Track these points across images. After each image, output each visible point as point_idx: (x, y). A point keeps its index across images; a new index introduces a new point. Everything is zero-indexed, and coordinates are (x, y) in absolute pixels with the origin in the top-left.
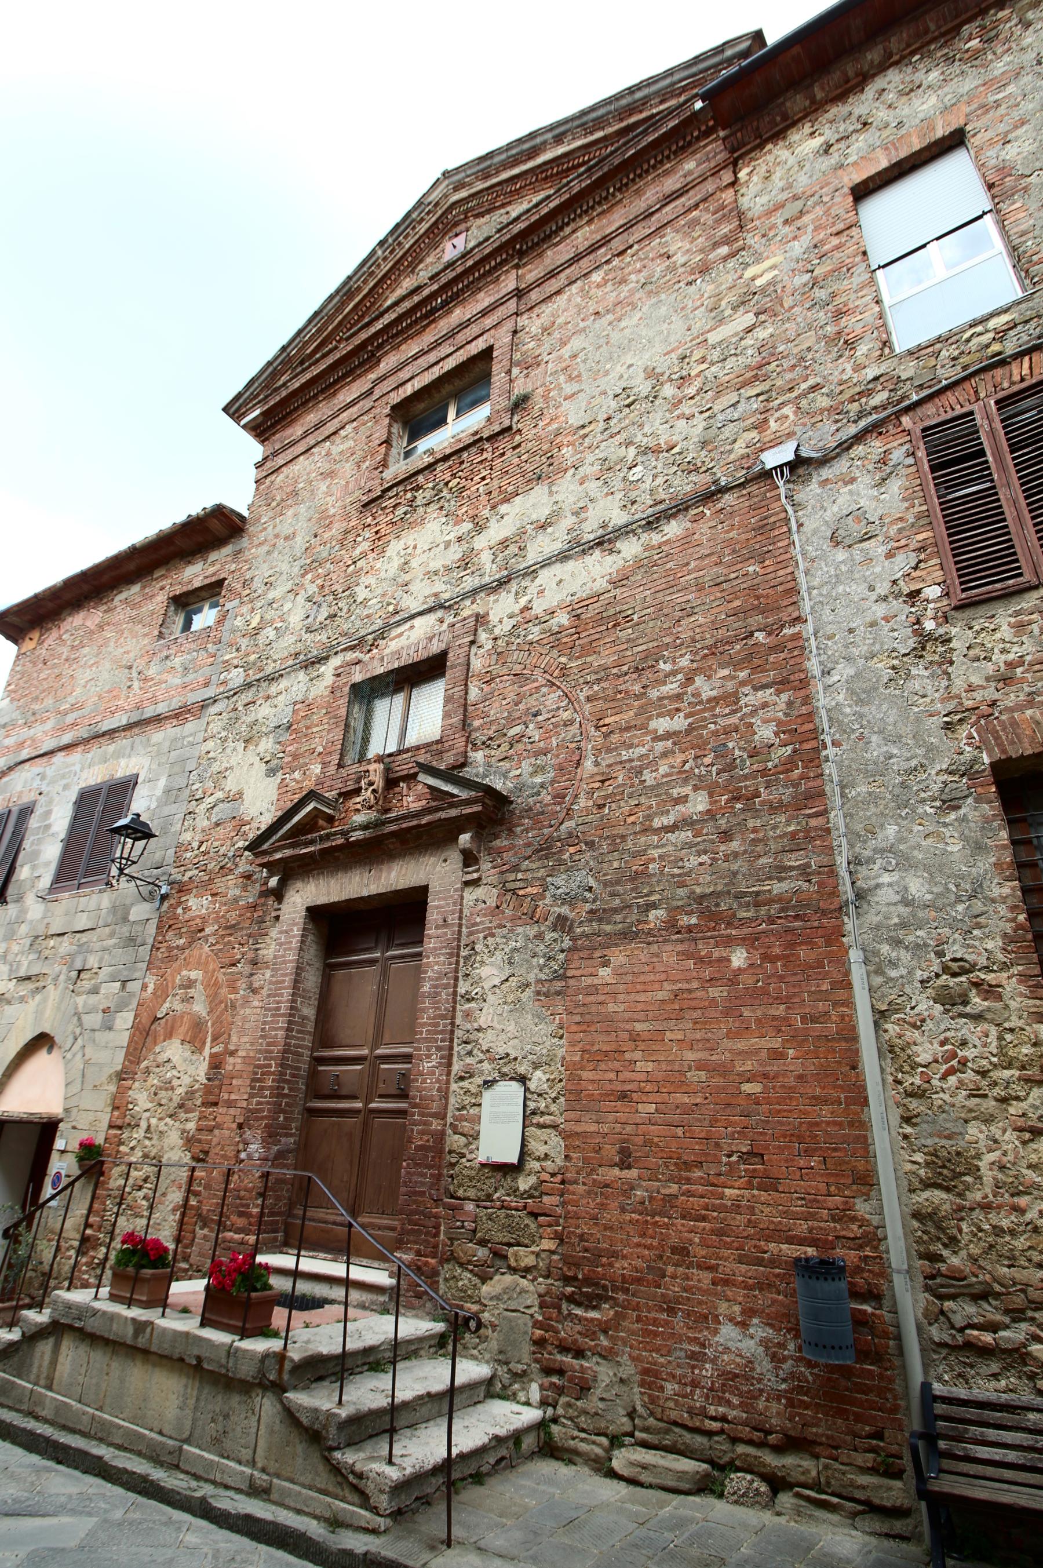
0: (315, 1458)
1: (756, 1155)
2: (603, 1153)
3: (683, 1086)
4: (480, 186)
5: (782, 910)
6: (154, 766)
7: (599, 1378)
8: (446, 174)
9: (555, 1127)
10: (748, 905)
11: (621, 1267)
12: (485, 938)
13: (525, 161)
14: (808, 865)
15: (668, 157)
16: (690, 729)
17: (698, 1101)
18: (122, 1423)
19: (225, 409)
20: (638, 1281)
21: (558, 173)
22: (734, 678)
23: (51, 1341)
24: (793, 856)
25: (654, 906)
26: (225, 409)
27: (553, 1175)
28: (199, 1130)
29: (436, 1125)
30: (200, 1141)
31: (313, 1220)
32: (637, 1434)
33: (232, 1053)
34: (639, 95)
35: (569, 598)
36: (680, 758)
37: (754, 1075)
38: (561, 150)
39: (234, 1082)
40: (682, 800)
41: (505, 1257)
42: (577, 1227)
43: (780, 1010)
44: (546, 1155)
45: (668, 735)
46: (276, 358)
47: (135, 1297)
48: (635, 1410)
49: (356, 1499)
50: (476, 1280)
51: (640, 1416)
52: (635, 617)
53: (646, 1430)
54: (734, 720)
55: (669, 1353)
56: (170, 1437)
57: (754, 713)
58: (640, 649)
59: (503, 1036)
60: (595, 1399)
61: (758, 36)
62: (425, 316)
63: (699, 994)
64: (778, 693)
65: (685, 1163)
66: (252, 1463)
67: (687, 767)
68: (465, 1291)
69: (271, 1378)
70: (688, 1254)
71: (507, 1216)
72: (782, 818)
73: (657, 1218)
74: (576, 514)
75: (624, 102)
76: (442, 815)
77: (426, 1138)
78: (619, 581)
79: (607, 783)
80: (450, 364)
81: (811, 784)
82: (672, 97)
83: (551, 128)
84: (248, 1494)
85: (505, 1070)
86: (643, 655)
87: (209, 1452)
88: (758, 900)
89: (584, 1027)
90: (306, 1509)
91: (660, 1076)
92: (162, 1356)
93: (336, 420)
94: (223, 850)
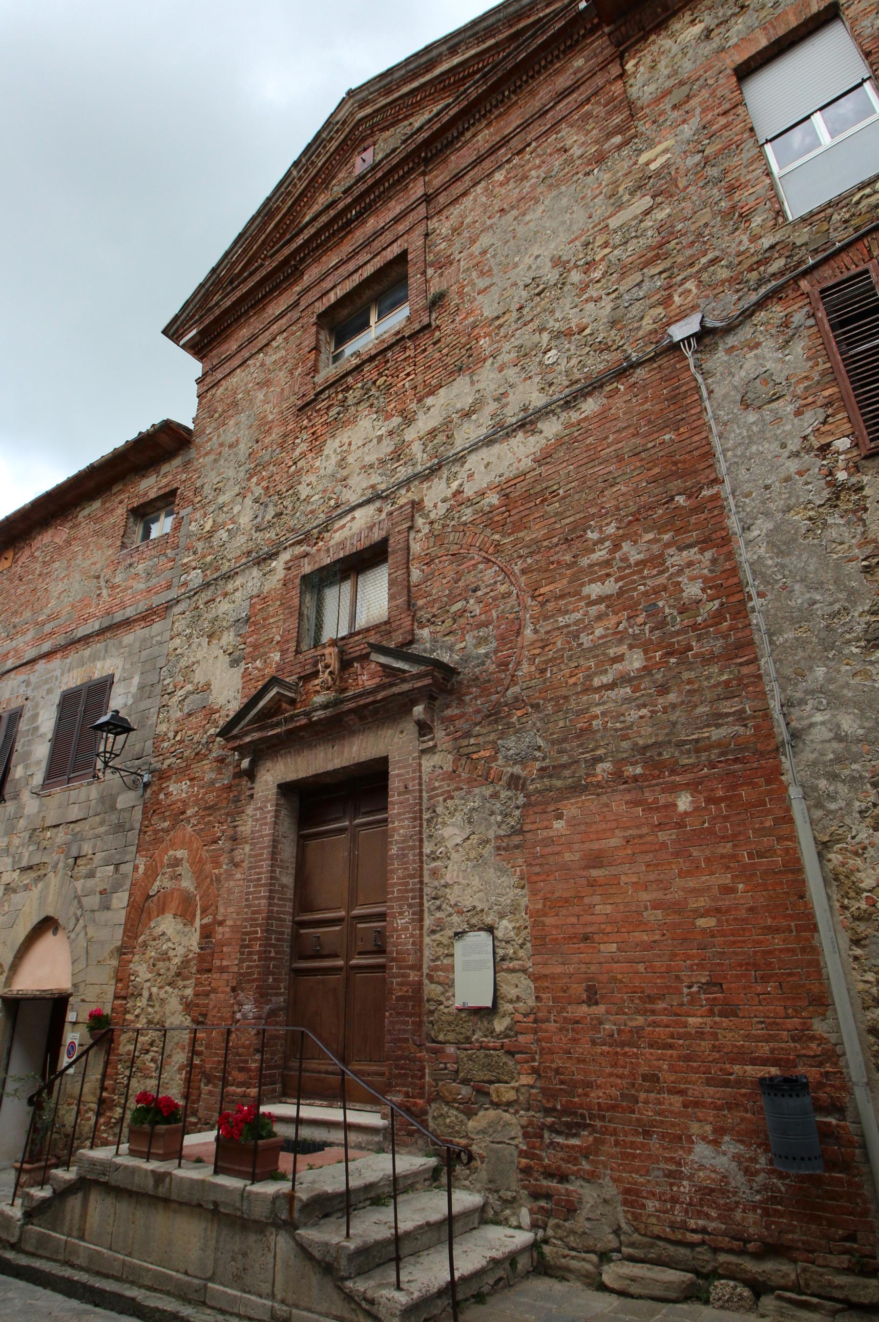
1: (715, 984)
3: (641, 925)
4: (383, 101)
5: (722, 754)
6: (127, 666)
7: (584, 1200)
8: (351, 93)
10: (689, 752)
11: (596, 1096)
12: (445, 800)
15: (558, 57)
16: (621, 592)
17: (656, 937)
18: (150, 1266)
19: (165, 332)
20: (613, 1108)
24: (728, 703)
25: (600, 759)
26: (165, 332)
28: (197, 995)
29: (413, 976)
30: (197, 1005)
31: (307, 1071)
32: (624, 1249)
35: (498, 479)
38: (456, 61)
39: (225, 949)
41: (487, 1094)
42: (553, 1061)
44: (518, 997)
45: (600, 600)
46: (207, 280)
50: (462, 1117)
52: (561, 492)
53: (632, 1245)
54: (662, 580)
55: (648, 1173)
56: (196, 1277)
57: (680, 572)
59: (469, 891)
62: (342, 229)
63: (649, 838)
64: (702, 551)
66: (272, 1296)
68: (453, 1128)
72: (715, 669)
73: (627, 1049)
76: (395, 690)
79: (547, 649)
80: (369, 270)
85: (474, 921)
88: (698, 747)
93: (267, 333)
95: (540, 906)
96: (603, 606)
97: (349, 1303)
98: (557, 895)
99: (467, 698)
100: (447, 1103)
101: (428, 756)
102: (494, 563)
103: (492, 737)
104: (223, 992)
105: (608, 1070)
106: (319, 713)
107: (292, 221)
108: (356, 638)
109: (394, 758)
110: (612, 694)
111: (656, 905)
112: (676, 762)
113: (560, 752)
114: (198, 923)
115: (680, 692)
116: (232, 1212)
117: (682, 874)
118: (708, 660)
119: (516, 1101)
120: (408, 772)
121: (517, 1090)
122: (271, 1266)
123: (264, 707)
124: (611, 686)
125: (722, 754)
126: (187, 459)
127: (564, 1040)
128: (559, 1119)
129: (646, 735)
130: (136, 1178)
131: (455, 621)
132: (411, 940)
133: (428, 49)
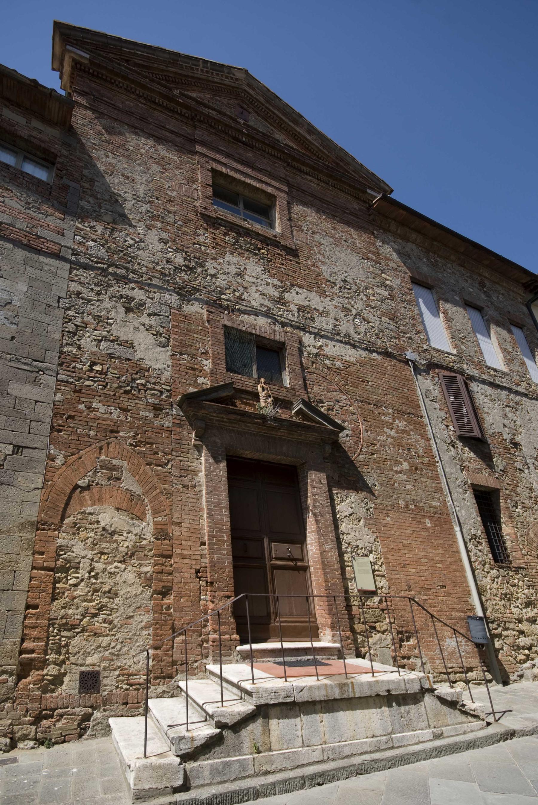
9: (383, 576)
23: (260, 721)
30: (161, 580)
61: (392, 191)
83: (309, 124)
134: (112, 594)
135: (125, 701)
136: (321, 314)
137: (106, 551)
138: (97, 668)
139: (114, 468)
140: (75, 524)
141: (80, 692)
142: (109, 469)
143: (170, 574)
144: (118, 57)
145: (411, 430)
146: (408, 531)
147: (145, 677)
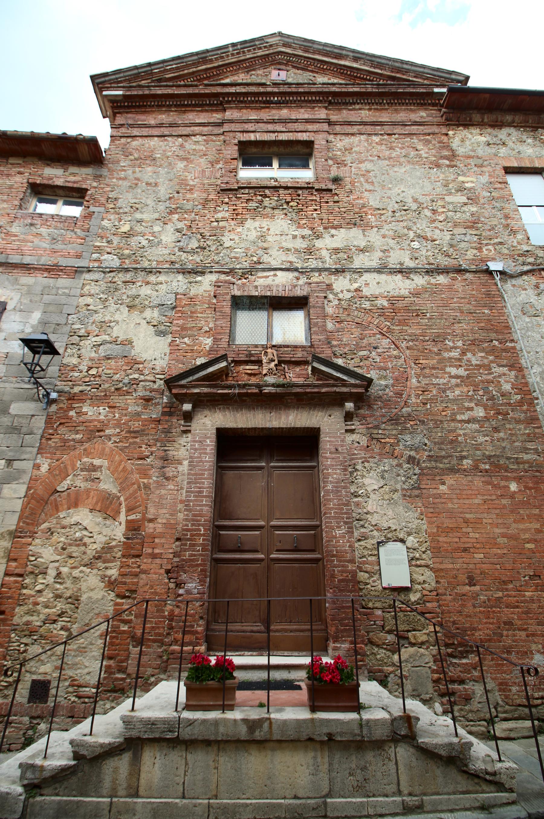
0: (453, 773)
1: (536, 576)
2: (459, 579)
3: (496, 545)
4: (301, 53)
5: (530, 467)
6: (26, 301)
7: (476, 692)
8: (280, 34)
9: (427, 566)
10: (513, 463)
11: (478, 635)
12: (363, 462)
13: (333, 58)
14: (537, 449)
15: (414, 104)
16: (468, 377)
17: (505, 552)
18: (249, 801)
19: (93, 78)
20: (489, 640)
21: (350, 75)
22: (487, 358)
23: (126, 757)
24: (530, 444)
25: (464, 457)
26: (93, 78)
27: (430, 591)
28: (122, 575)
29: (350, 567)
30: (125, 583)
31: (232, 631)
32: (500, 715)
33: (151, 521)
34: (405, 66)
35: (386, 293)
36: (466, 389)
37: (530, 540)
38: (355, 65)
39: (157, 540)
40: (471, 409)
41: (407, 638)
42: (450, 617)
43: (537, 511)
44: (424, 581)
45: (457, 377)
46: (142, 67)
47: (225, 703)
48: (498, 704)
49: (492, 788)
50: (389, 653)
51: (501, 706)
52: (428, 314)
53: (505, 712)
54: (490, 377)
55: (511, 673)
56: (309, 798)
57: (500, 376)
58: (434, 331)
59: (385, 517)
60: (476, 703)
61: (467, 78)
62: (264, 102)
63: (496, 502)
64: (510, 370)
65: (503, 581)
66: (399, 793)
67: (470, 394)
68: (382, 661)
69: (403, 733)
70: (512, 624)
71: (405, 616)
72: (522, 427)
73: (494, 609)
74: (384, 251)
75: (397, 64)
76: (337, 390)
77: (345, 575)
78: (416, 294)
79: (426, 393)
80: (283, 137)
81: (532, 414)
82: (421, 78)
83: (354, 51)
84: (403, 814)
85: (389, 535)
86: (436, 335)
87: (354, 797)
88: (518, 461)
89: (436, 515)
90: (457, 807)
91: (484, 540)
92: (279, 741)
93: (188, 129)
94: (116, 377)
95: (435, 530)
96: (459, 380)
97: (472, 780)
98: (445, 525)
99: (375, 407)
100: (378, 646)
101: (349, 434)
102: (388, 337)
103: (394, 432)
104: (156, 573)
105: (485, 621)
106: (270, 388)
107: (218, 75)
108: (286, 349)
109: (325, 429)
110: (469, 426)
111: (504, 536)
112: (508, 467)
113: (440, 449)
114: (122, 517)
115: (506, 433)
116: (351, 739)
117: (515, 522)
118: (518, 422)
119: (427, 641)
120: (337, 441)
121: (428, 635)
122: (395, 771)
123: (211, 373)
124: (468, 421)
125: (530, 467)
126: (98, 173)
127: (457, 605)
128: (456, 649)
129: (490, 450)
130: (221, 729)
131: (361, 361)
132: (348, 544)
133: (341, 48)
134: (75, 600)
135: (70, 715)
136: (362, 251)
137: (74, 555)
138: (49, 677)
139: (94, 468)
140: (50, 529)
141: (29, 702)
142: (88, 470)
143: (136, 575)
144: (149, 81)
145: (492, 362)
146: (476, 501)
147: (94, 690)
